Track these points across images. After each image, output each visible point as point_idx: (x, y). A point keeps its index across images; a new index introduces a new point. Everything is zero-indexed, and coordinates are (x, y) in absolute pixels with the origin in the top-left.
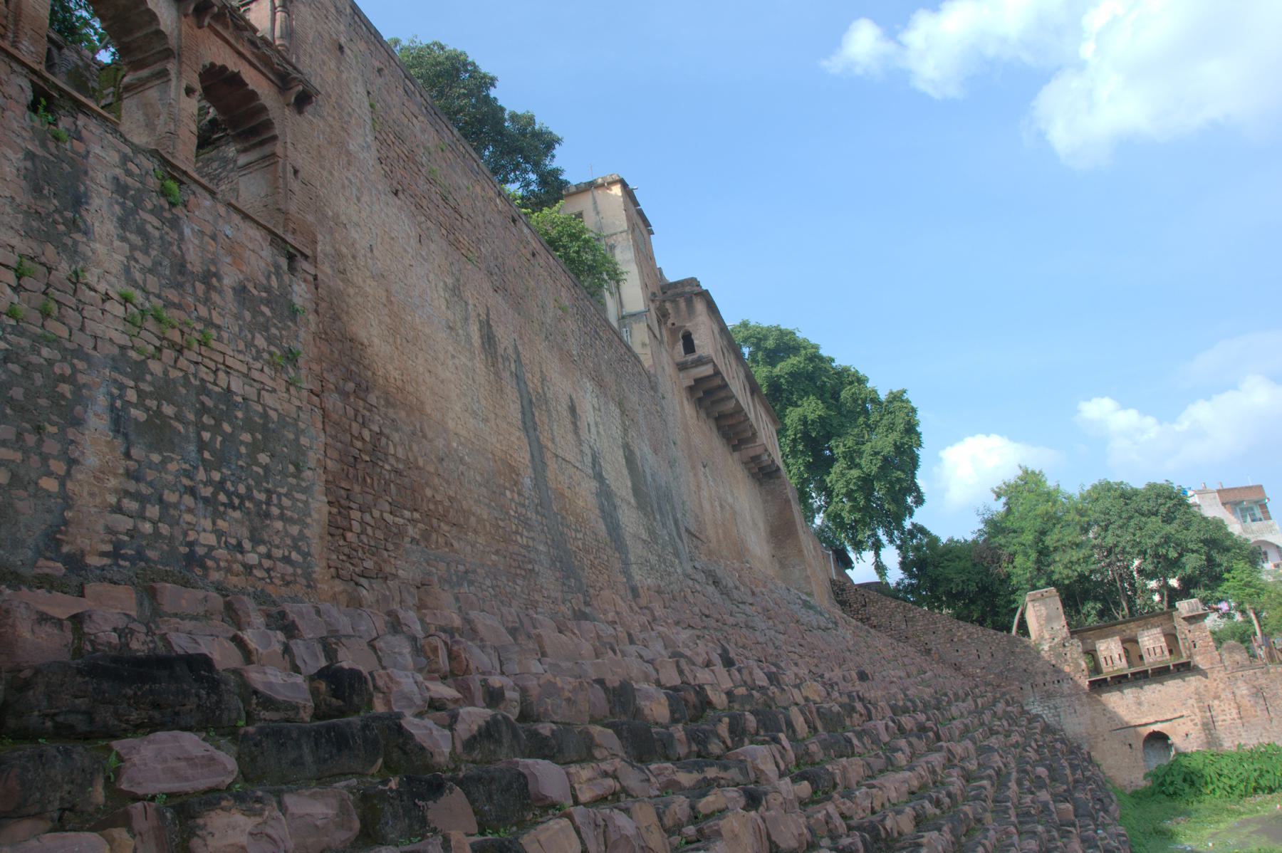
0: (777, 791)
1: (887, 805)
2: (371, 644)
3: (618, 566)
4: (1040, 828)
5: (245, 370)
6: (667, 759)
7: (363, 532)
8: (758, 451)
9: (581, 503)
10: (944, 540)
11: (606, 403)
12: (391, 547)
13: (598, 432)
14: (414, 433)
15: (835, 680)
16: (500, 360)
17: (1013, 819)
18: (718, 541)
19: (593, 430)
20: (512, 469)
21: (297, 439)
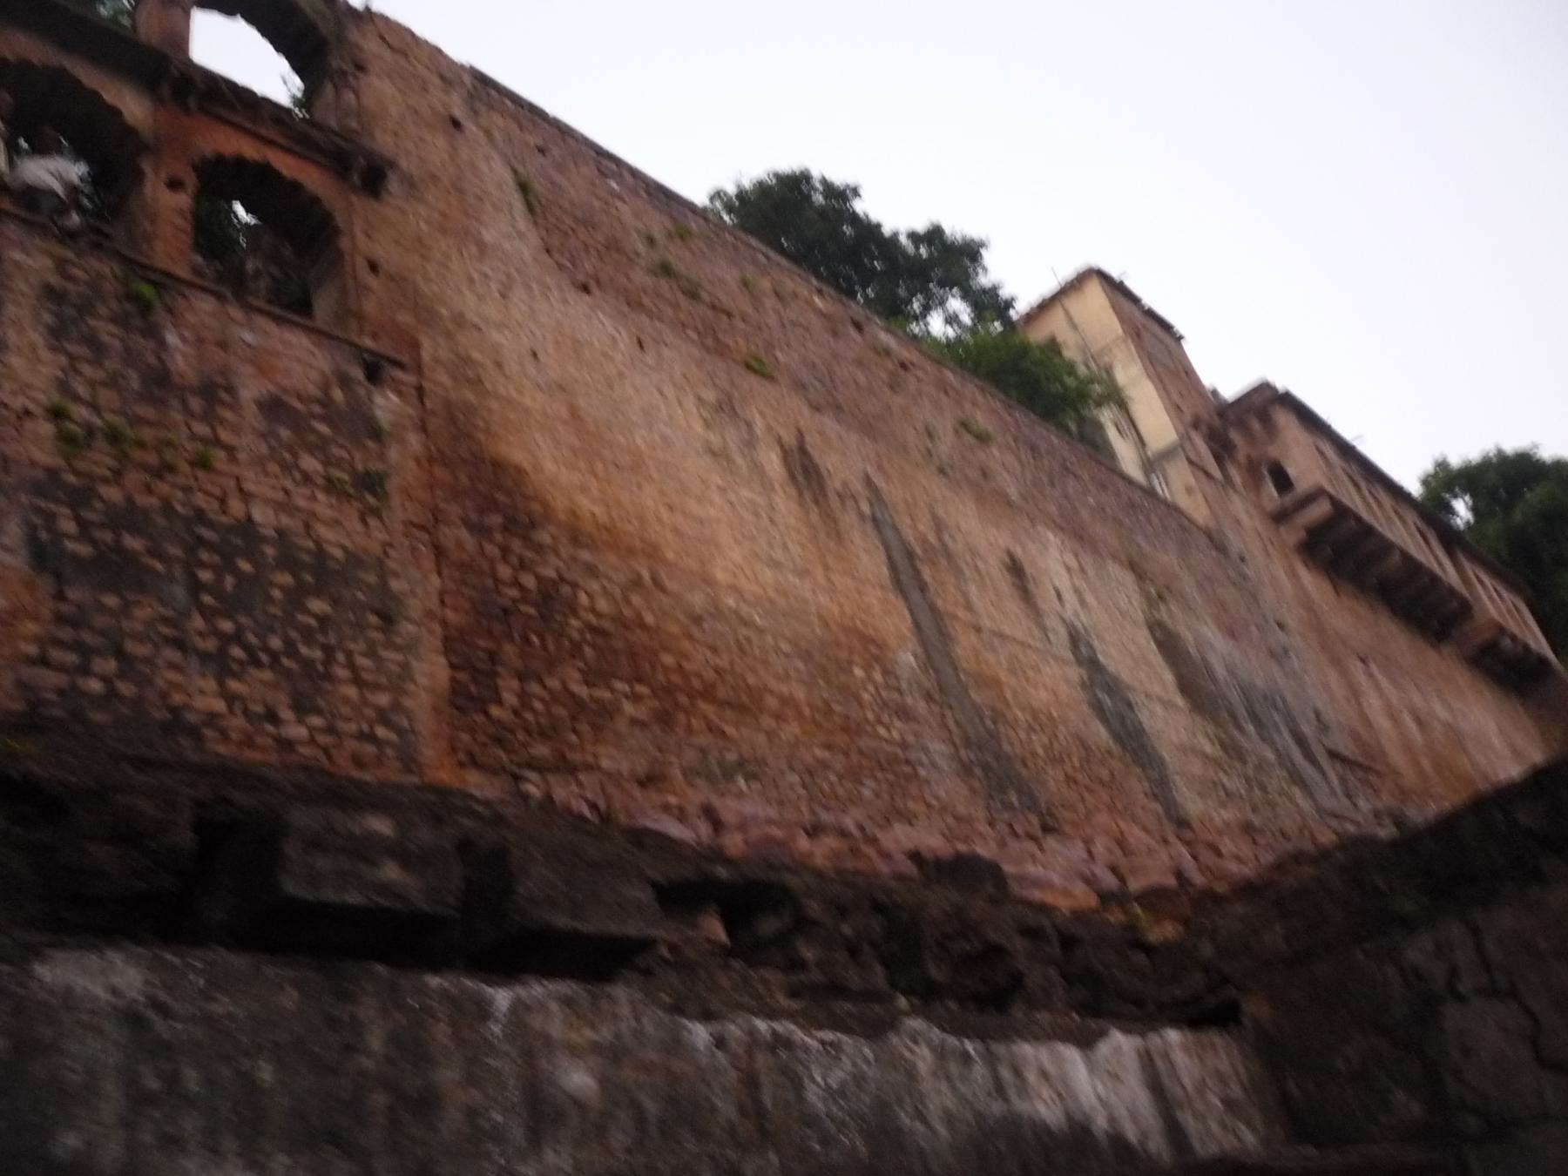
5: (280, 495)
18: (1421, 773)
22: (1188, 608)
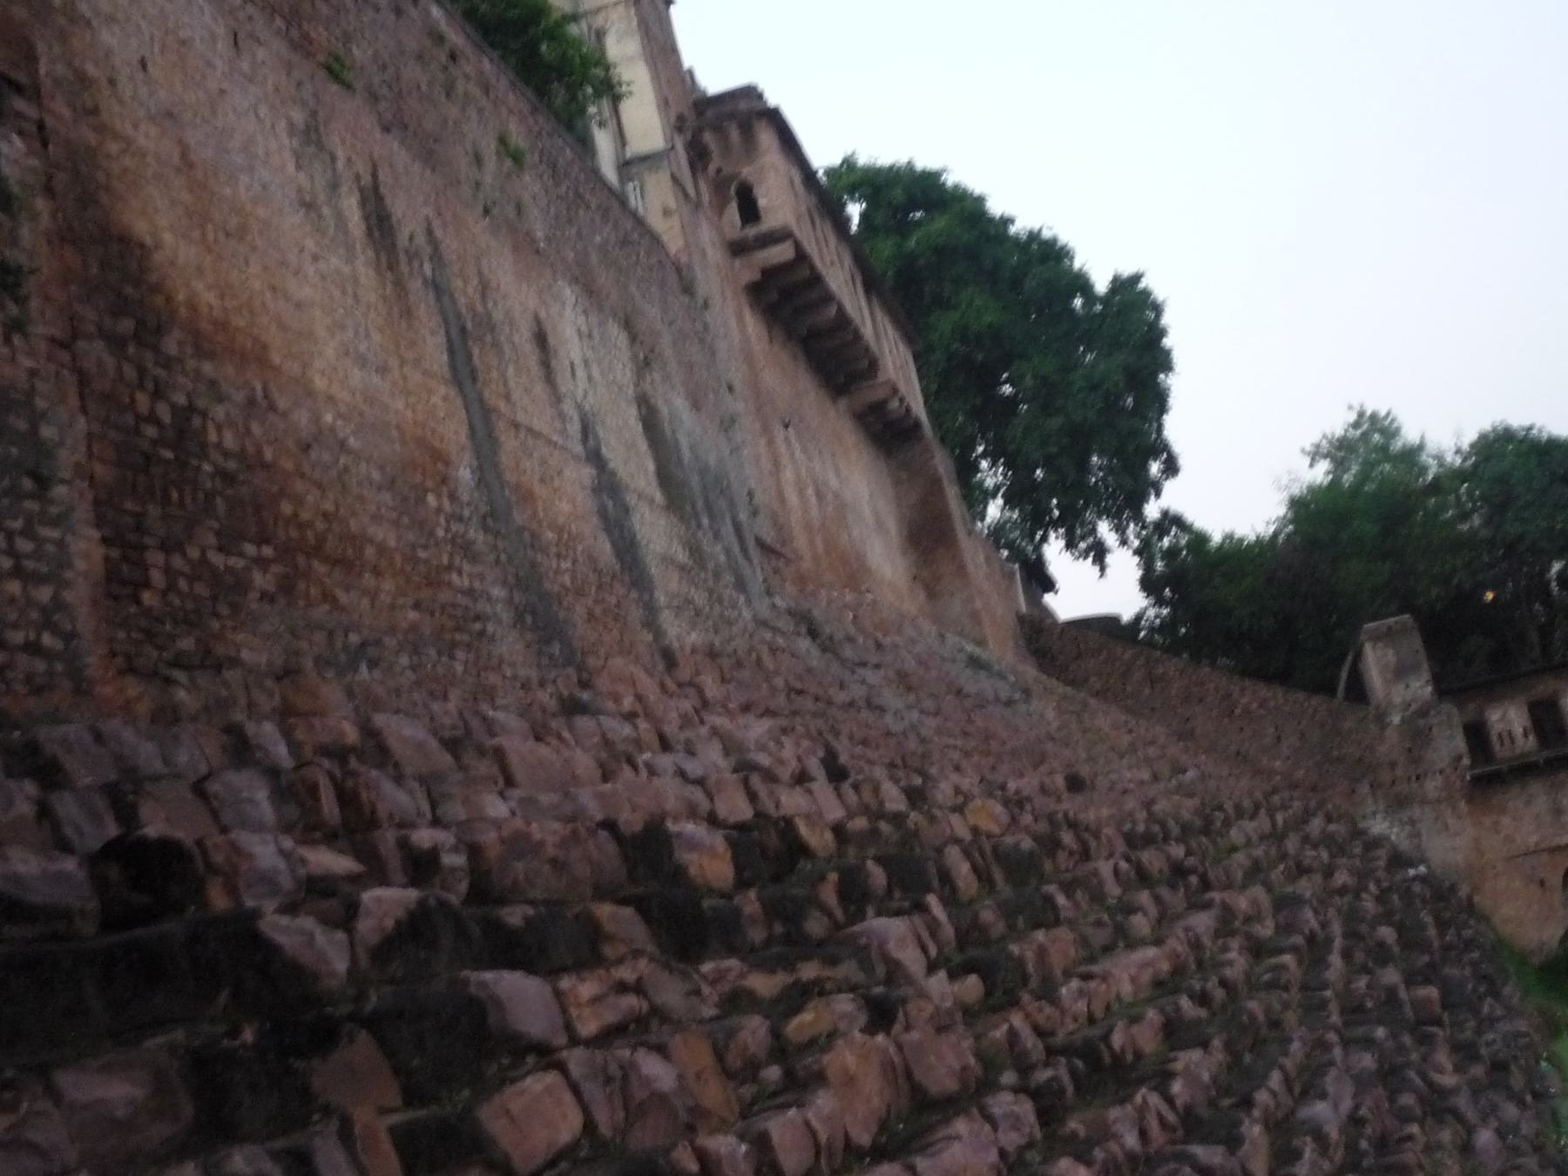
0: (923, 995)
1: (1115, 1007)
2: (199, 789)
3: (636, 614)
4: (1380, 1032)
6: (732, 951)
7: (171, 587)
8: (879, 394)
9: (565, 506)
10: (1217, 538)
11: (602, 324)
12: (224, 610)
13: (590, 379)
14: (251, 402)
15: (1025, 793)
16: (403, 258)
17: (1335, 1018)
18: (815, 558)
19: (581, 373)
20: (439, 457)
21: (34, 430)
22: (667, 378)
